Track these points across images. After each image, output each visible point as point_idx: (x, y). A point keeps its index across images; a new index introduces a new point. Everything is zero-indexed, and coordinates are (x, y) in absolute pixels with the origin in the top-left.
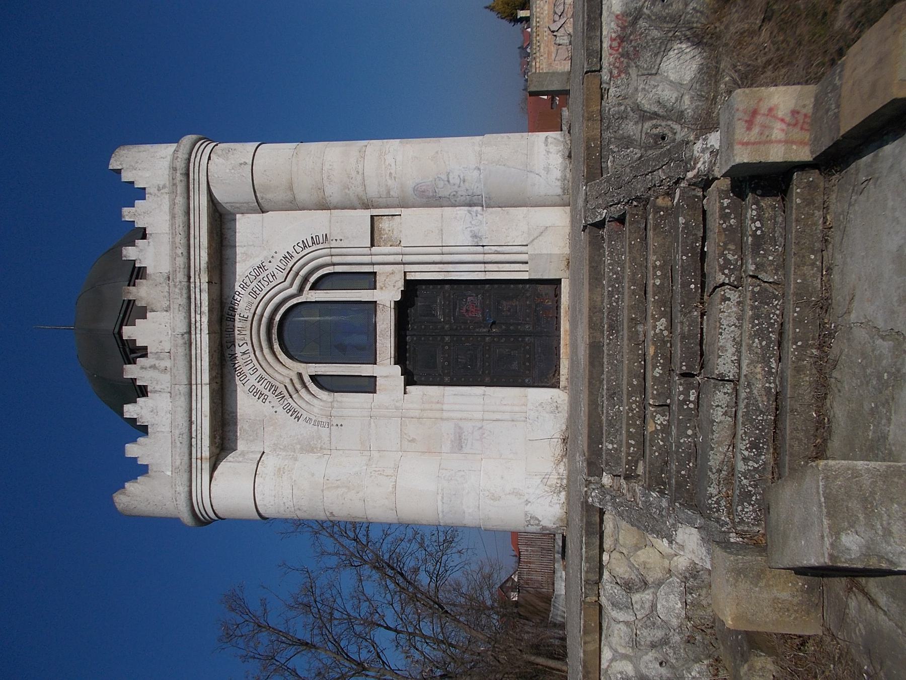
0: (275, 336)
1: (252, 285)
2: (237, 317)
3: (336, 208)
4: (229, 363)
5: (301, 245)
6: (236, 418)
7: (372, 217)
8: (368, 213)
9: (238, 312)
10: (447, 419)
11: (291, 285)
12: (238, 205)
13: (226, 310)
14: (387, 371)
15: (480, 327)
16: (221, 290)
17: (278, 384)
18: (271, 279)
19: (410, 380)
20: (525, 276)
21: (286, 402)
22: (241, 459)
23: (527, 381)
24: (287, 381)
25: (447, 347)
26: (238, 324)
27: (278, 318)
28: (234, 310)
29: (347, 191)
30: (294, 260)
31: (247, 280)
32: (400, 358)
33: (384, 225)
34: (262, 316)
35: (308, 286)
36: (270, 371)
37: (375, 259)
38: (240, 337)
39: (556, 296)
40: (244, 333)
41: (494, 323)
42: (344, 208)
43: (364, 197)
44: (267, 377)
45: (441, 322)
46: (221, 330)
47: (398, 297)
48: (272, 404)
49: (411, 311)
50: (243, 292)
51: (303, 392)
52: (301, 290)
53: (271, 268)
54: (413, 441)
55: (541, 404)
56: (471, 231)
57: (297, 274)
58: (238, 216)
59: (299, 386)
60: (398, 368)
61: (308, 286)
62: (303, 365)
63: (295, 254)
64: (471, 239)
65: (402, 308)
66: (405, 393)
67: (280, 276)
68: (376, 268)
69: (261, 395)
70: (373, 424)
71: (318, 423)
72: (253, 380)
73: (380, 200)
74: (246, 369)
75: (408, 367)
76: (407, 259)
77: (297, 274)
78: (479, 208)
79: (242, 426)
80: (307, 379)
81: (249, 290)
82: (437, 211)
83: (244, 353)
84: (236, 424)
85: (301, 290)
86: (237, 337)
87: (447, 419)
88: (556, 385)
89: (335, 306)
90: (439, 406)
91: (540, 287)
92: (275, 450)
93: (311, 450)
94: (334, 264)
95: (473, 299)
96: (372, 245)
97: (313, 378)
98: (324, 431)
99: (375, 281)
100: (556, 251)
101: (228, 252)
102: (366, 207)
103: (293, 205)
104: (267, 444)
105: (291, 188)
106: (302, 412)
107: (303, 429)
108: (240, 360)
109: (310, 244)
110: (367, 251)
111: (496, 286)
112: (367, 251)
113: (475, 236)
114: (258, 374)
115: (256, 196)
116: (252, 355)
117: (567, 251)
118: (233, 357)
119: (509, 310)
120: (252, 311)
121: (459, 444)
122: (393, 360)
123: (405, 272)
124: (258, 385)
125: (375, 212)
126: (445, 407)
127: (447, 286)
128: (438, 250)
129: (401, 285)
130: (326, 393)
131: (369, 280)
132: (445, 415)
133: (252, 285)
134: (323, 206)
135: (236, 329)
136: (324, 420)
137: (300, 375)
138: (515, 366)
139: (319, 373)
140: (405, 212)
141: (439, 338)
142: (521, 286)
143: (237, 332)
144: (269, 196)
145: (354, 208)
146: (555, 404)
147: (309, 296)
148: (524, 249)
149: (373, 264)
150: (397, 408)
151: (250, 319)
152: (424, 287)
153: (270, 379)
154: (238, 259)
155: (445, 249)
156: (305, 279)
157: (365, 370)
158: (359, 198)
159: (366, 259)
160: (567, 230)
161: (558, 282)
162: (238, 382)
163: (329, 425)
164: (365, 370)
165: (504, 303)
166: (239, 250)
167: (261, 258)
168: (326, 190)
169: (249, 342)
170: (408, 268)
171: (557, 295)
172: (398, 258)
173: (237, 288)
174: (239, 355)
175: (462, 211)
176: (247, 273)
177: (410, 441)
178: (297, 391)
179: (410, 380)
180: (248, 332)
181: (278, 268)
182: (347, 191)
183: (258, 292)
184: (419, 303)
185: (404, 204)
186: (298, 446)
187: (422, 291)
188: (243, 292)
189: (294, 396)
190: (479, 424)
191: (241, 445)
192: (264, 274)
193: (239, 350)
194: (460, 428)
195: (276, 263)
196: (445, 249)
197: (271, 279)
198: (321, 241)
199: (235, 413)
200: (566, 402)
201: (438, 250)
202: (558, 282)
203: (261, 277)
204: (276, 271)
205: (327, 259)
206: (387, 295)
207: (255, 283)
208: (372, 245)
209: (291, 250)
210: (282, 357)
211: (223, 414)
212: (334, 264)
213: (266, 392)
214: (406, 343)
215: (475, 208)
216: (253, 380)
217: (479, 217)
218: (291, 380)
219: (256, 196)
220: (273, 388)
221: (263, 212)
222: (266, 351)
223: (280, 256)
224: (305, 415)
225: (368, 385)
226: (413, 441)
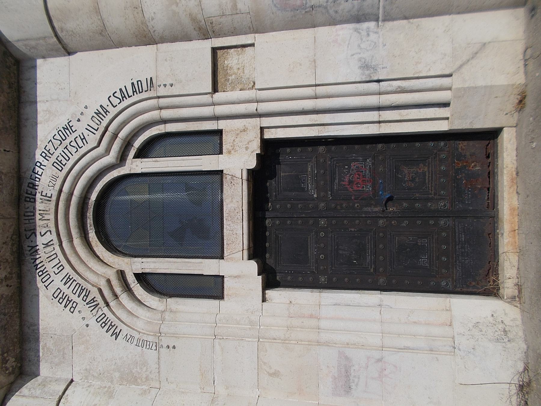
0: (90, 221)
1: (57, 153)
2: (38, 196)
3: (163, 40)
4: (28, 258)
5: (118, 95)
6: (38, 329)
7: (214, 51)
8: (207, 45)
9: (40, 189)
10: (327, 344)
11: (108, 151)
12: (33, 43)
13: (25, 186)
14: (238, 268)
15: (370, 205)
16: (19, 161)
17: (89, 287)
18: (81, 144)
19: (270, 280)
20: (443, 127)
21: (100, 313)
22: (38, 392)
23: (443, 283)
24: (103, 284)
25: (322, 234)
26: (39, 206)
27: (94, 196)
28: (34, 186)
29: (174, 7)
30: (110, 116)
31: (50, 146)
32: (257, 250)
33: (231, 61)
34: (71, 194)
35: (132, 153)
36: (80, 268)
37: (220, 110)
38: (42, 223)
39: (488, 157)
40: (47, 217)
41: (390, 199)
42: (174, 39)
43: (200, 17)
44: (76, 277)
45: (313, 199)
46: (19, 215)
47: (252, 164)
48: (83, 315)
49: (271, 184)
50: (45, 162)
51: (124, 298)
52: (122, 158)
53: (80, 128)
54: (275, 374)
55: (476, 325)
56: (360, 60)
57: (115, 136)
58: (39, 62)
59: (118, 290)
60: (253, 266)
61: (132, 153)
62: (127, 260)
63: (110, 108)
64: (359, 71)
65: (259, 180)
66: (264, 300)
67: (92, 140)
68: (222, 125)
69: (67, 303)
70: (217, 347)
71: (142, 343)
72: (57, 281)
73: (223, 20)
74: (49, 267)
75: (268, 261)
76: (264, 107)
77: (115, 136)
78: (372, 25)
79: (46, 344)
80: (131, 279)
81: (53, 159)
82: (306, 34)
83: (47, 245)
84: (37, 340)
85: (122, 158)
86: (39, 223)
87: (327, 344)
88: (491, 291)
89: (169, 179)
90: (313, 322)
91: (462, 145)
92: (86, 377)
93: (134, 380)
94: (165, 121)
95: (361, 164)
96: (215, 89)
97: (141, 277)
98: (151, 355)
99: (221, 144)
100: (502, 80)
101: (27, 110)
102: (205, 34)
103: (105, 40)
104: (76, 369)
105: (97, 11)
106: (121, 326)
107: (120, 351)
108: (42, 254)
109: (131, 93)
110: (207, 99)
111: (393, 145)
112: (207, 99)
113: (365, 66)
114: (64, 273)
115: (53, 28)
116: (57, 248)
117: (520, 79)
118: (34, 250)
119: (413, 180)
120: (57, 187)
121: (345, 382)
122: (246, 253)
123: (262, 129)
124: (64, 288)
125: (218, 42)
126: (323, 324)
127: (321, 149)
128: (309, 91)
129: (256, 147)
130: (157, 299)
131: (211, 140)
132: (324, 337)
133: (57, 153)
134: (146, 38)
135: (38, 212)
136: (150, 339)
137: (121, 275)
138: (424, 260)
139: (147, 271)
140: (259, 39)
141: (311, 222)
142: (431, 144)
143: (38, 217)
144: (71, 25)
145: (187, 38)
146: (501, 326)
147: (134, 166)
148: (445, 81)
149: (217, 118)
150: (251, 323)
151: (54, 198)
152: (288, 150)
153: (80, 280)
154: (40, 118)
155: (320, 90)
156: (127, 144)
157: (207, 267)
158: (194, 19)
159: (207, 111)
160: (520, 47)
161: (492, 135)
162: (40, 285)
163: (158, 347)
164: (207, 267)
165: (406, 170)
166: (41, 107)
167: (68, 116)
168: (145, 9)
169: (53, 230)
170: (266, 122)
171: (491, 157)
172: (251, 108)
173: (39, 158)
174: (40, 247)
175: (345, 31)
176: (50, 137)
177: (271, 375)
178: (116, 296)
179: (270, 280)
180: (52, 217)
181: (92, 130)
182: (174, 7)
183: (64, 162)
184: (283, 172)
185: (258, 28)
186: (117, 375)
187: (287, 156)
188: (45, 162)
189: (112, 304)
190: (377, 355)
191: (44, 369)
192: (71, 138)
193: (40, 241)
194: (347, 358)
195: (86, 120)
196: (320, 90)
197: (81, 144)
198: (145, 88)
199: (36, 325)
200: (519, 322)
201: (309, 91)
202: (492, 135)
203: (67, 141)
204: (86, 133)
205: (154, 115)
206: (238, 160)
207: (60, 150)
208: (215, 89)
209: (105, 103)
210: (100, 249)
211: (21, 326)
212: (165, 121)
213: (74, 298)
214: (265, 229)
215: (365, 25)
216: (57, 281)
217: (373, 37)
218: (109, 281)
219: (53, 28)
220: (83, 292)
221: (69, 54)
222: (77, 241)
223: (91, 112)
224: (125, 330)
225: (211, 288)
226: (275, 374)
